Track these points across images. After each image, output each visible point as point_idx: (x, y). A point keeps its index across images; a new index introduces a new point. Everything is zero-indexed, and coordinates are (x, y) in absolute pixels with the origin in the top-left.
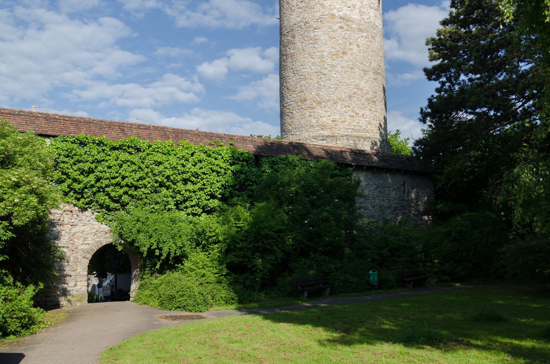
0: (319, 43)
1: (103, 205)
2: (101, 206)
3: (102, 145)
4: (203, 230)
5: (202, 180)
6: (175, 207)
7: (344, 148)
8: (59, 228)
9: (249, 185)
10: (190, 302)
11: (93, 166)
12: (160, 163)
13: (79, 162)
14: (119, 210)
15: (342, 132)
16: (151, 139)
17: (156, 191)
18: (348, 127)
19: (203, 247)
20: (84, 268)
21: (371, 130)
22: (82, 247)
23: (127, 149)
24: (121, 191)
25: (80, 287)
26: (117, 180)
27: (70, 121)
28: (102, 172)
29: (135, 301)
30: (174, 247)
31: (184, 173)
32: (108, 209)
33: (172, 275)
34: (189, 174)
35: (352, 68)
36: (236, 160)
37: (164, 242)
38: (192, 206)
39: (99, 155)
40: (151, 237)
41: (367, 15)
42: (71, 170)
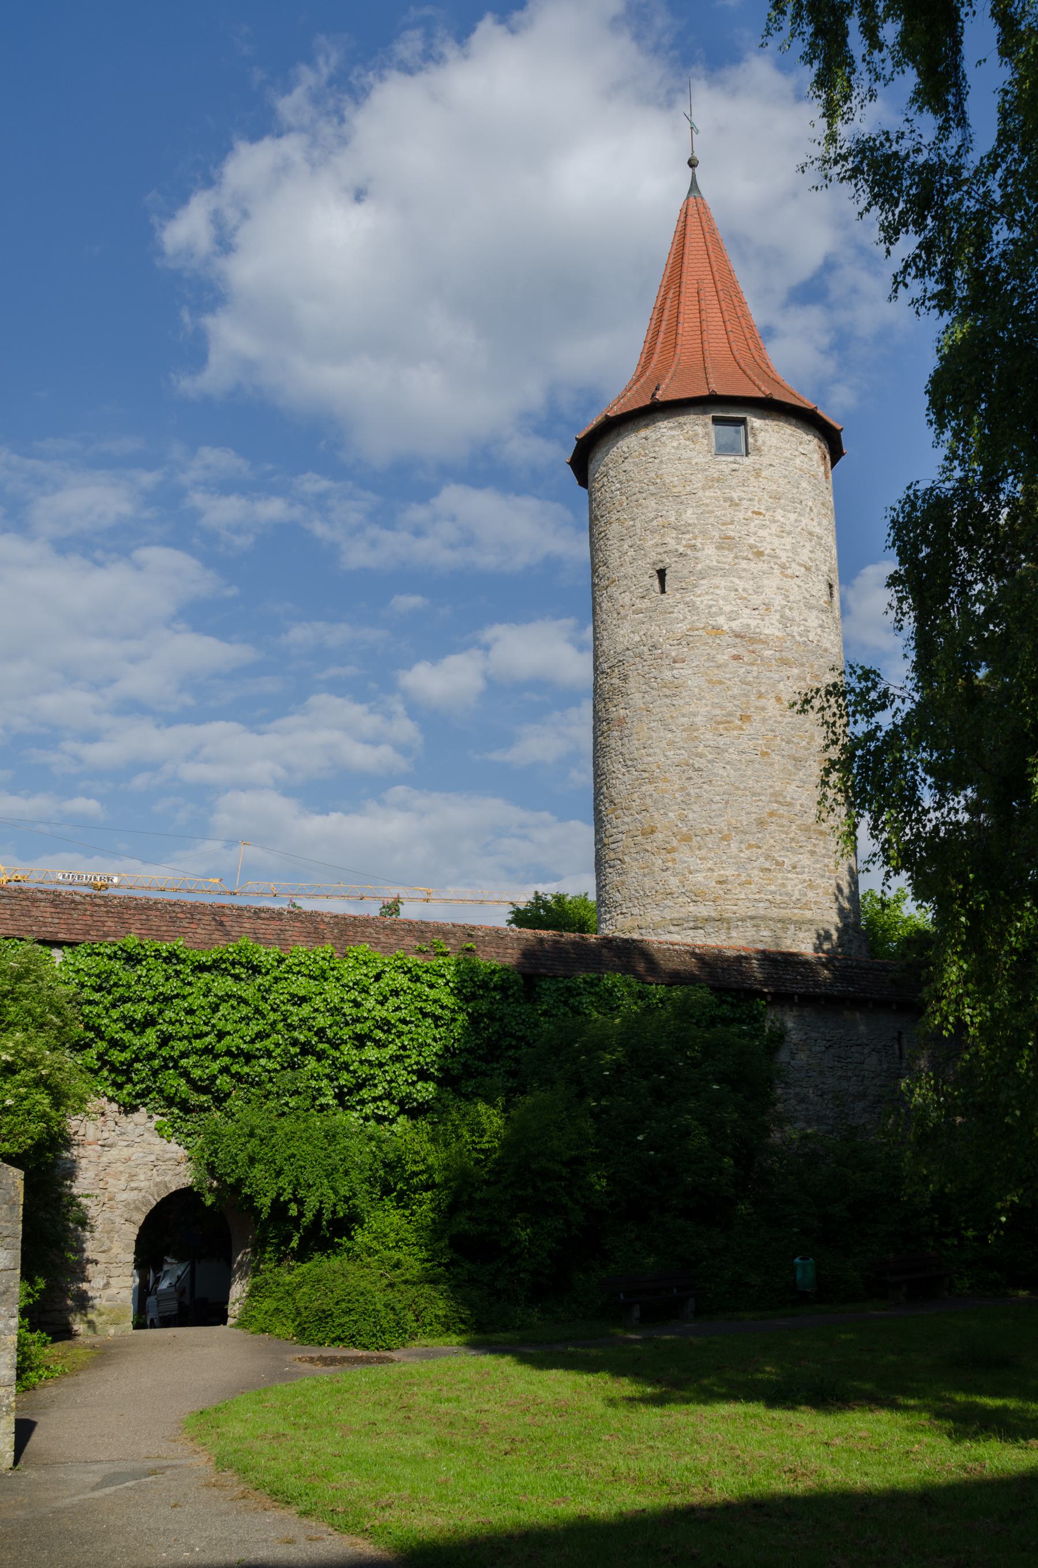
0: (684, 694)
1: (173, 1098)
2: (170, 1101)
3: (174, 961)
4: (400, 1158)
5: (399, 1037)
6: (336, 1102)
7: (744, 949)
8: (75, 1153)
9: (510, 1047)
10: (366, 1326)
11: (154, 1009)
12: (304, 999)
13: (125, 1002)
14: (208, 1109)
15: (742, 910)
16: (284, 944)
17: (294, 1063)
18: (757, 896)
19: (399, 1198)
20: (128, 1246)
21: (816, 903)
22: (124, 1196)
23: (230, 968)
24: (216, 1066)
25: (116, 1291)
26: (207, 1040)
27: (105, 906)
28: (173, 1024)
29: (240, 1324)
30: (332, 1196)
31: (357, 1020)
32: (185, 1107)
33: (327, 1264)
34: (369, 1023)
35: (764, 754)
36: (480, 987)
37: (310, 1186)
38: (375, 1100)
39: (168, 985)
40: (279, 1173)
41: (799, 625)
42: (106, 1021)
